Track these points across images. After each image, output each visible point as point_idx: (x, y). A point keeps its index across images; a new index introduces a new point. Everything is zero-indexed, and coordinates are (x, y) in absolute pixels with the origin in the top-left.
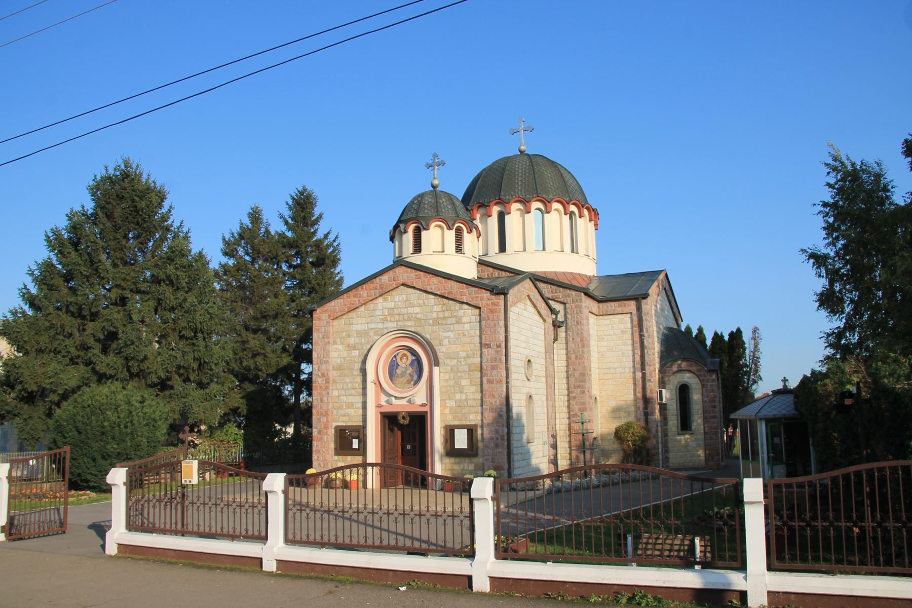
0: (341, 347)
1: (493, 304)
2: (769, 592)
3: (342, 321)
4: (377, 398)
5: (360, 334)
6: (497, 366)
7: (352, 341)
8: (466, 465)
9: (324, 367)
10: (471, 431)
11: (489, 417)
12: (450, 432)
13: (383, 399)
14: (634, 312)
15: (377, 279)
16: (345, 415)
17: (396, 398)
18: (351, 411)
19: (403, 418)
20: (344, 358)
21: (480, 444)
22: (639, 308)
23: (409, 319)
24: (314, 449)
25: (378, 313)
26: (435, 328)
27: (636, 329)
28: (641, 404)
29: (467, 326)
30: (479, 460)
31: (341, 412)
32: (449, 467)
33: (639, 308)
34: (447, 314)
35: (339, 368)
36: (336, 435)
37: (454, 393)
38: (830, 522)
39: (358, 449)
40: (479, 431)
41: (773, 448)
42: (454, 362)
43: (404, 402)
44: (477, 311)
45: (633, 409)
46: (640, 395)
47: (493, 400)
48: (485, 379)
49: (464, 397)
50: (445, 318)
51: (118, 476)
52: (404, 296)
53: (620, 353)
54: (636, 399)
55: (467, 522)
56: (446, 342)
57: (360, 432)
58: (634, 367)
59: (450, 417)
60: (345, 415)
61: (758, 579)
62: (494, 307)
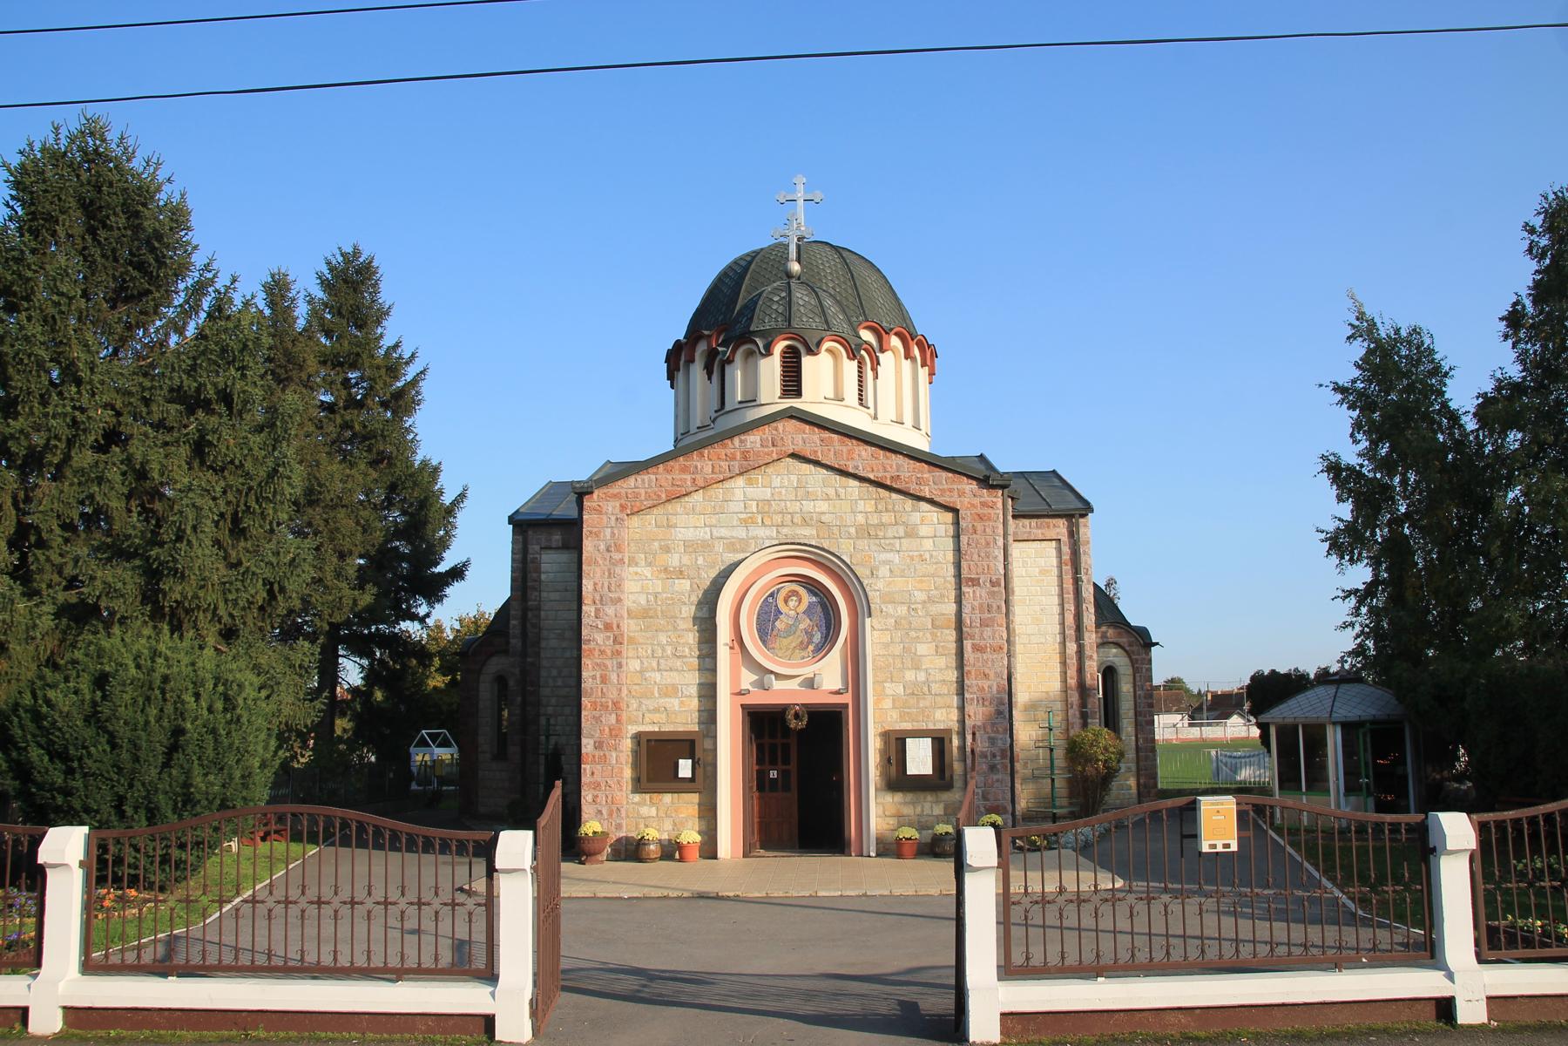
0: (647, 572)
1: (983, 504)
2: (1489, 998)
3: (651, 518)
4: (735, 678)
5: (691, 547)
6: (992, 619)
7: (674, 560)
8: (927, 806)
9: (610, 610)
10: (940, 744)
11: (977, 714)
12: (896, 745)
13: (747, 679)
14: (1065, 538)
15: (736, 440)
16: (656, 710)
17: (778, 676)
18: (674, 703)
19: (797, 716)
20: (656, 595)
21: (957, 767)
22: (1073, 534)
23: (805, 523)
24: (586, 779)
25: (733, 507)
26: (863, 544)
27: (1067, 568)
28: (1074, 698)
29: (928, 544)
30: (953, 796)
31: (649, 703)
32: (891, 810)
33: (1073, 534)
34: (887, 518)
35: (645, 614)
36: (636, 754)
37: (902, 670)
38: (1500, 888)
39: (692, 780)
40: (956, 742)
41: (1351, 773)
42: (902, 610)
43: (793, 685)
44: (949, 516)
45: (1059, 706)
46: (1072, 682)
47: (986, 684)
48: (968, 644)
49: (922, 677)
50: (882, 525)
51: (65, 847)
52: (794, 478)
53: (1037, 608)
54: (1065, 689)
55: (95, 937)
56: (884, 571)
57: (696, 745)
58: (1063, 633)
59: (895, 715)
60: (656, 710)
61: (1472, 982)
62: (986, 511)
